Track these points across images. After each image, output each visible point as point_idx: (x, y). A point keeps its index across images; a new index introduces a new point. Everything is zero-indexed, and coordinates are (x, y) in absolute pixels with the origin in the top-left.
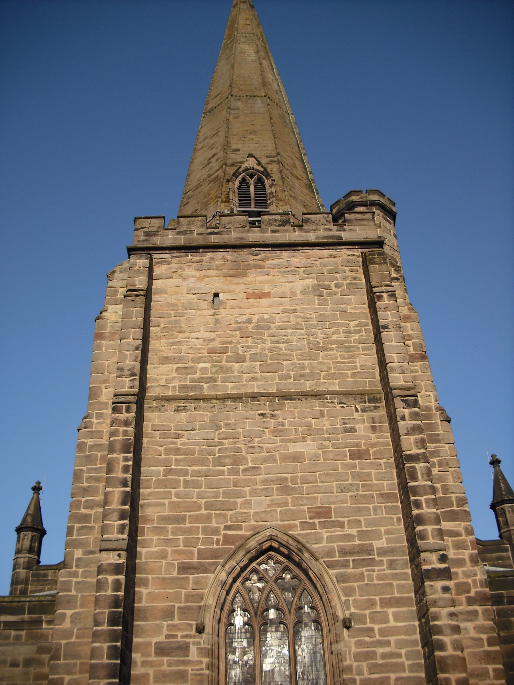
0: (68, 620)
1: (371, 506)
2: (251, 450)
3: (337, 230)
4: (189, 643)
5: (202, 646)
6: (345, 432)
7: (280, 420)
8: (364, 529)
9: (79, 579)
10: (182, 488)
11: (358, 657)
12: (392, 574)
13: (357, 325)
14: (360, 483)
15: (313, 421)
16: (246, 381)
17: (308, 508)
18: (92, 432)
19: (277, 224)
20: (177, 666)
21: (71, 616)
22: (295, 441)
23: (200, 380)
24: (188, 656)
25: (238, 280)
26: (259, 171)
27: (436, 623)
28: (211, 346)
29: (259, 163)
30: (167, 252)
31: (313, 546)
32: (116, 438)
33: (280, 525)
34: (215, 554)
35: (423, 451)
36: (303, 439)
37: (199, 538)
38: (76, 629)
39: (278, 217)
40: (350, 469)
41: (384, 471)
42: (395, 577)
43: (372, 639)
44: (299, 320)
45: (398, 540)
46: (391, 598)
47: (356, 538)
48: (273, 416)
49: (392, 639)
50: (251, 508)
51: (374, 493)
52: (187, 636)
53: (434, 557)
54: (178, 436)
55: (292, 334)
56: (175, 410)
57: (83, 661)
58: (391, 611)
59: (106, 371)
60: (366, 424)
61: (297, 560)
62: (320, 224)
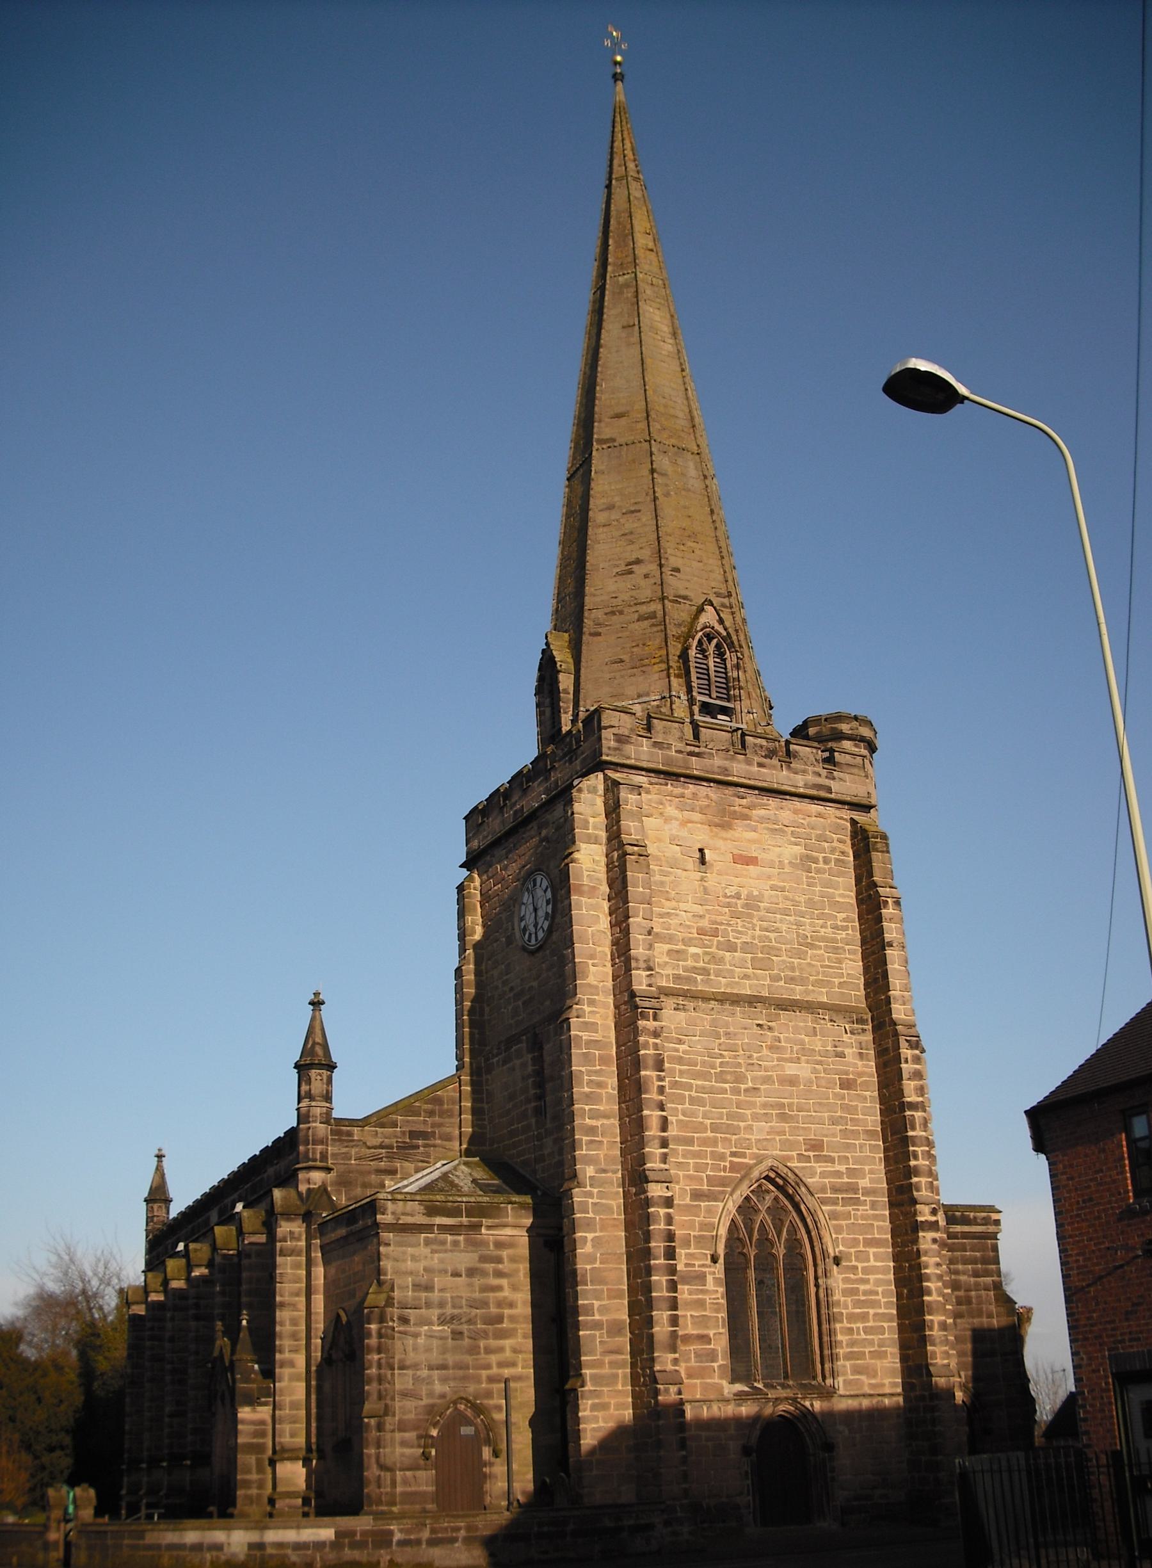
0: (589, 1244)
1: (857, 1142)
2: (750, 1067)
3: (827, 777)
4: (705, 1272)
5: (717, 1276)
6: (836, 1056)
7: (776, 1034)
8: (851, 1166)
9: (595, 1200)
10: (687, 1105)
11: (846, 1292)
12: (873, 1215)
13: (844, 920)
14: (849, 1116)
15: (807, 1039)
16: (739, 977)
17: (804, 1139)
18: (586, 1023)
19: (763, 754)
20: (697, 1295)
21: (592, 1240)
22: (791, 1060)
23: (694, 970)
24: (705, 1285)
25: (724, 834)
26: (719, 634)
27: (926, 1271)
28: (701, 925)
29: (721, 621)
30: (643, 773)
31: (809, 1180)
32: (647, 1052)
33: (779, 1155)
34: (723, 1182)
35: (921, 1099)
36: (798, 1060)
37: (708, 1164)
38: (598, 1255)
39: (764, 742)
40: (839, 1100)
41: (868, 1105)
42: (876, 1217)
43: (856, 1277)
44: (788, 902)
45: (878, 1181)
46: (872, 1238)
47: (845, 1176)
48: (770, 1028)
49: (872, 1277)
50: (753, 1134)
51: (860, 1128)
52: (703, 1266)
53: (926, 1209)
54: (680, 1042)
55: (781, 921)
56: (675, 1009)
57: (609, 1287)
58: (872, 1250)
59: (591, 942)
60: (854, 1049)
61: (791, 1192)
62: (809, 764)
